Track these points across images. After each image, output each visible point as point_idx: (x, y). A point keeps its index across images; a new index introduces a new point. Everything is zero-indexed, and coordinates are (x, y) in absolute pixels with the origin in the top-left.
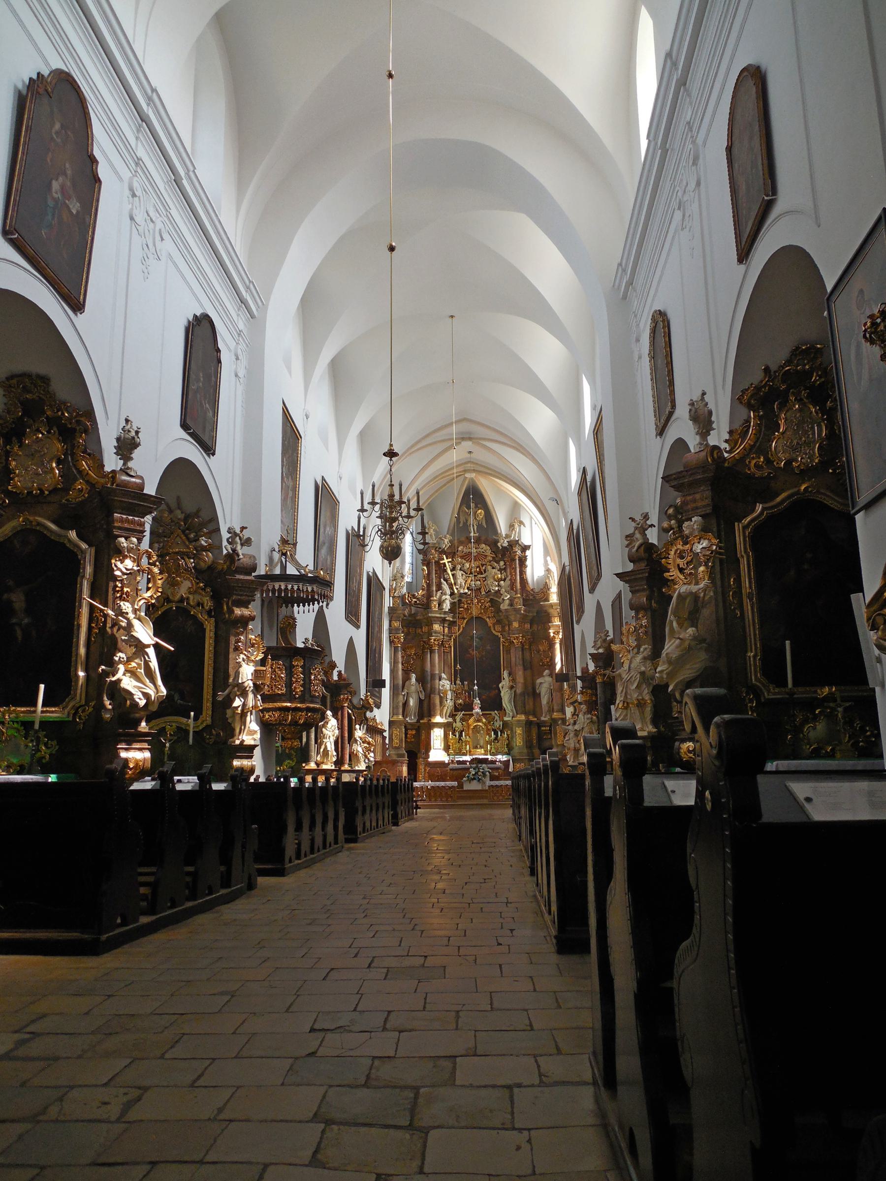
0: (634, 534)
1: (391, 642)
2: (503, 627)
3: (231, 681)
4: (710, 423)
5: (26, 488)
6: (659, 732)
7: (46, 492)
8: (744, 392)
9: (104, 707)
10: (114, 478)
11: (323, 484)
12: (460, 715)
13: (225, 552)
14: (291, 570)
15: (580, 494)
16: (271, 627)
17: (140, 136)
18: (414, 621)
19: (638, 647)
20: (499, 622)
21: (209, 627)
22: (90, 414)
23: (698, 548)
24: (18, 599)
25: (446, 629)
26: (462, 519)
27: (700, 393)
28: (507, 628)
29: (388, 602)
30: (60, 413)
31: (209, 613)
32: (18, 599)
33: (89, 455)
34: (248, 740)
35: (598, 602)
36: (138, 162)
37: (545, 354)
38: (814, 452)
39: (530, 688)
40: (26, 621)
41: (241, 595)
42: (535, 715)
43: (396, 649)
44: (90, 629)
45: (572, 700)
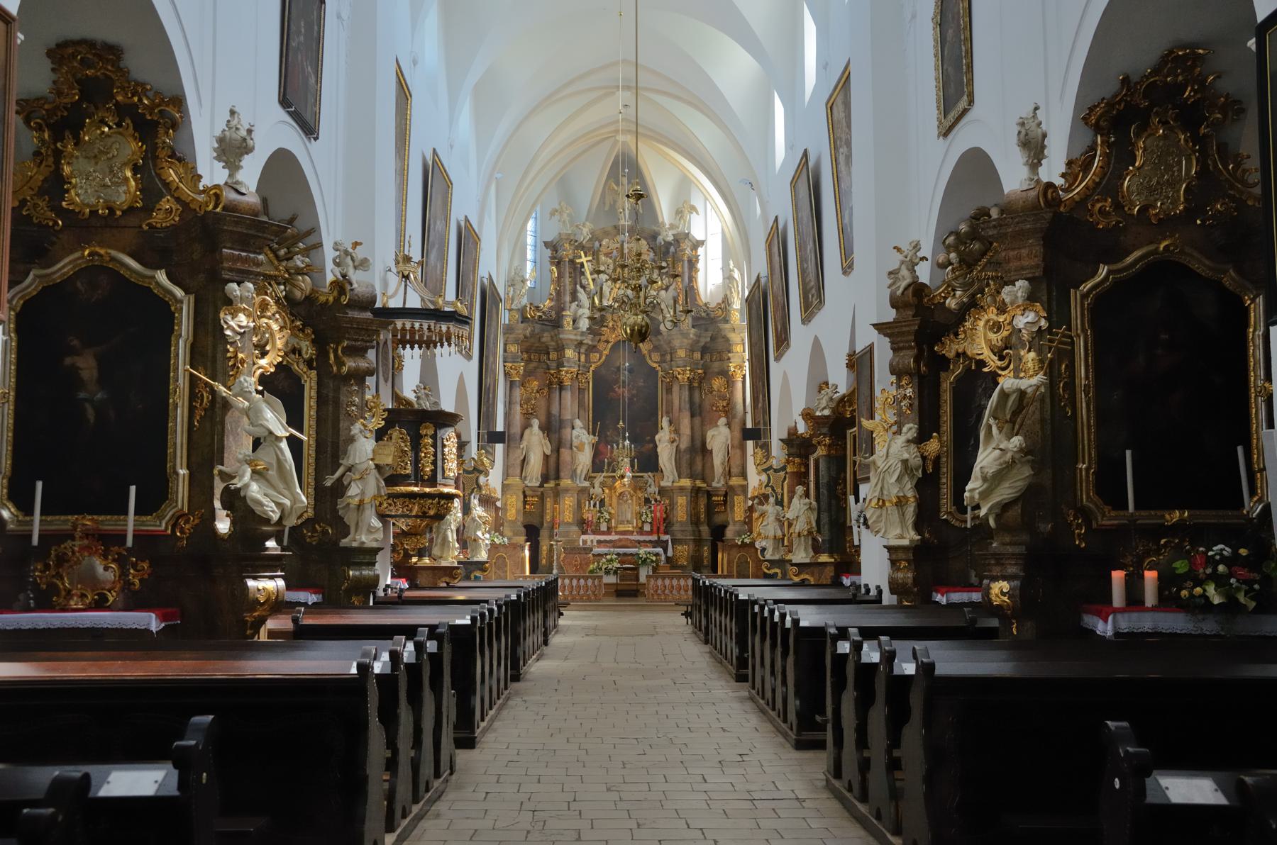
0: (899, 269)
1: (506, 374)
2: (663, 355)
4: (1043, 147)
5: (88, 205)
7: (119, 213)
8: (1091, 109)
10: (217, 196)
11: (434, 161)
12: (600, 478)
14: (414, 302)
15: (794, 183)
16: (386, 381)
22: (179, 101)
23: (1020, 322)
24: (87, 366)
25: (583, 358)
28: (668, 358)
29: (504, 318)
30: (136, 99)
31: (309, 364)
32: (87, 366)
34: (364, 539)
38: (1179, 197)
39: (698, 443)
40: (99, 396)
41: (356, 340)
42: (704, 480)
43: (512, 383)
45: (765, 466)
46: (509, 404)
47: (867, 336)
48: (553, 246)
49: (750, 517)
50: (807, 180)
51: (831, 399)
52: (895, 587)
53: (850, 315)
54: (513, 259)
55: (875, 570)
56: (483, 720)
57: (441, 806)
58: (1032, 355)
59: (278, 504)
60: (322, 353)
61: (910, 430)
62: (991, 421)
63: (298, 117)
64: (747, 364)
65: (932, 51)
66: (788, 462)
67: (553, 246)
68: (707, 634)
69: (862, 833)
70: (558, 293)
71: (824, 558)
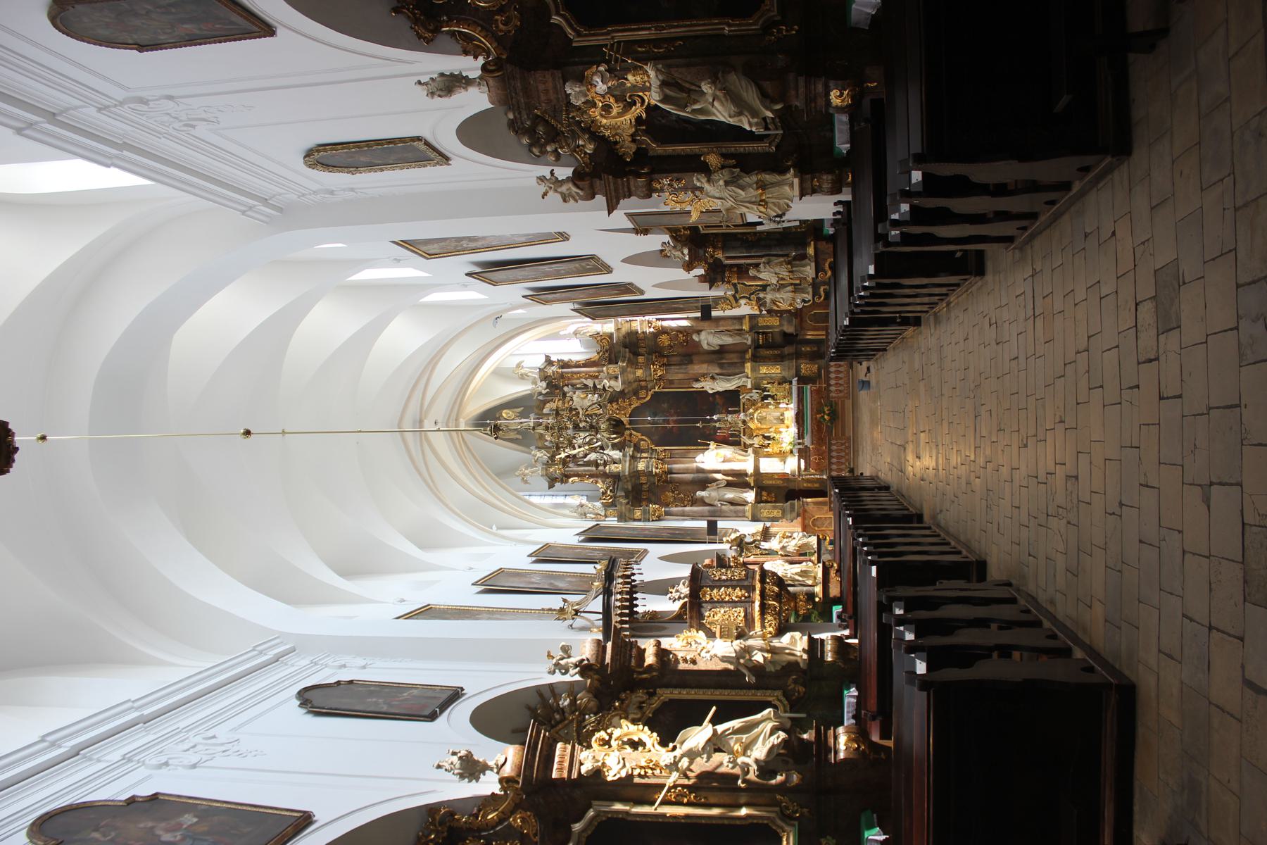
0: (561, 193)
1: (659, 519)
2: (642, 388)
3: (731, 667)
4: (452, 75)
6: (794, 166)
8: (420, 37)
9: (783, 784)
12: (745, 439)
13: (578, 678)
14: (597, 604)
16: (664, 628)
17: (95, 757)
18: (637, 492)
19: (695, 189)
20: (636, 393)
21: (666, 694)
22: (431, 809)
23: (601, 87)
25: (644, 455)
26: (513, 435)
27: (419, 87)
29: (612, 521)
31: (651, 695)
33: (479, 811)
35: (624, 261)
36: (127, 759)
37: (328, 324)
39: (714, 356)
42: (746, 352)
43: (667, 514)
44: (689, 804)
46: (683, 515)
47: (619, 218)
48: (552, 482)
49: (776, 312)
50: (491, 271)
51: (674, 247)
52: (836, 190)
53: (603, 234)
54: (564, 517)
55: (821, 208)
56: (959, 553)
57: (1042, 598)
58: (630, 77)
59: (772, 734)
60: (642, 684)
61: (699, 180)
62: (688, 109)
63: (444, 706)
64: (647, 318)
65: (379, 174)
66: (729, 282)
67: (552, 482)
68: (878, 350)
69: (1066, 217)
70: (591, 476)
71: (811, 251)
